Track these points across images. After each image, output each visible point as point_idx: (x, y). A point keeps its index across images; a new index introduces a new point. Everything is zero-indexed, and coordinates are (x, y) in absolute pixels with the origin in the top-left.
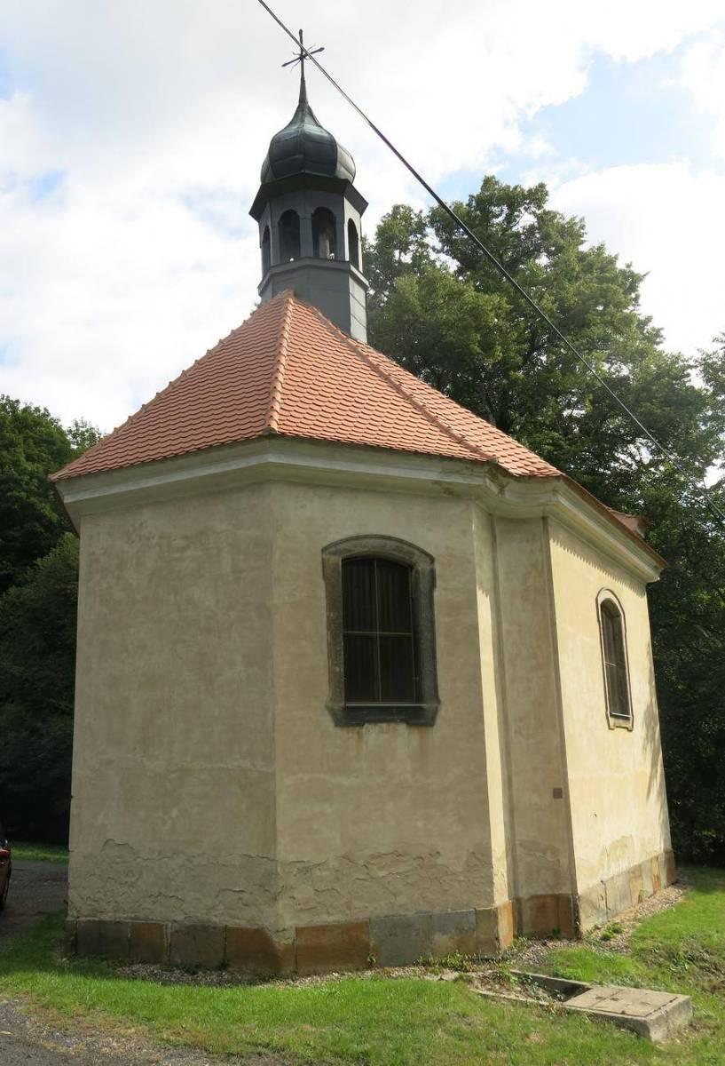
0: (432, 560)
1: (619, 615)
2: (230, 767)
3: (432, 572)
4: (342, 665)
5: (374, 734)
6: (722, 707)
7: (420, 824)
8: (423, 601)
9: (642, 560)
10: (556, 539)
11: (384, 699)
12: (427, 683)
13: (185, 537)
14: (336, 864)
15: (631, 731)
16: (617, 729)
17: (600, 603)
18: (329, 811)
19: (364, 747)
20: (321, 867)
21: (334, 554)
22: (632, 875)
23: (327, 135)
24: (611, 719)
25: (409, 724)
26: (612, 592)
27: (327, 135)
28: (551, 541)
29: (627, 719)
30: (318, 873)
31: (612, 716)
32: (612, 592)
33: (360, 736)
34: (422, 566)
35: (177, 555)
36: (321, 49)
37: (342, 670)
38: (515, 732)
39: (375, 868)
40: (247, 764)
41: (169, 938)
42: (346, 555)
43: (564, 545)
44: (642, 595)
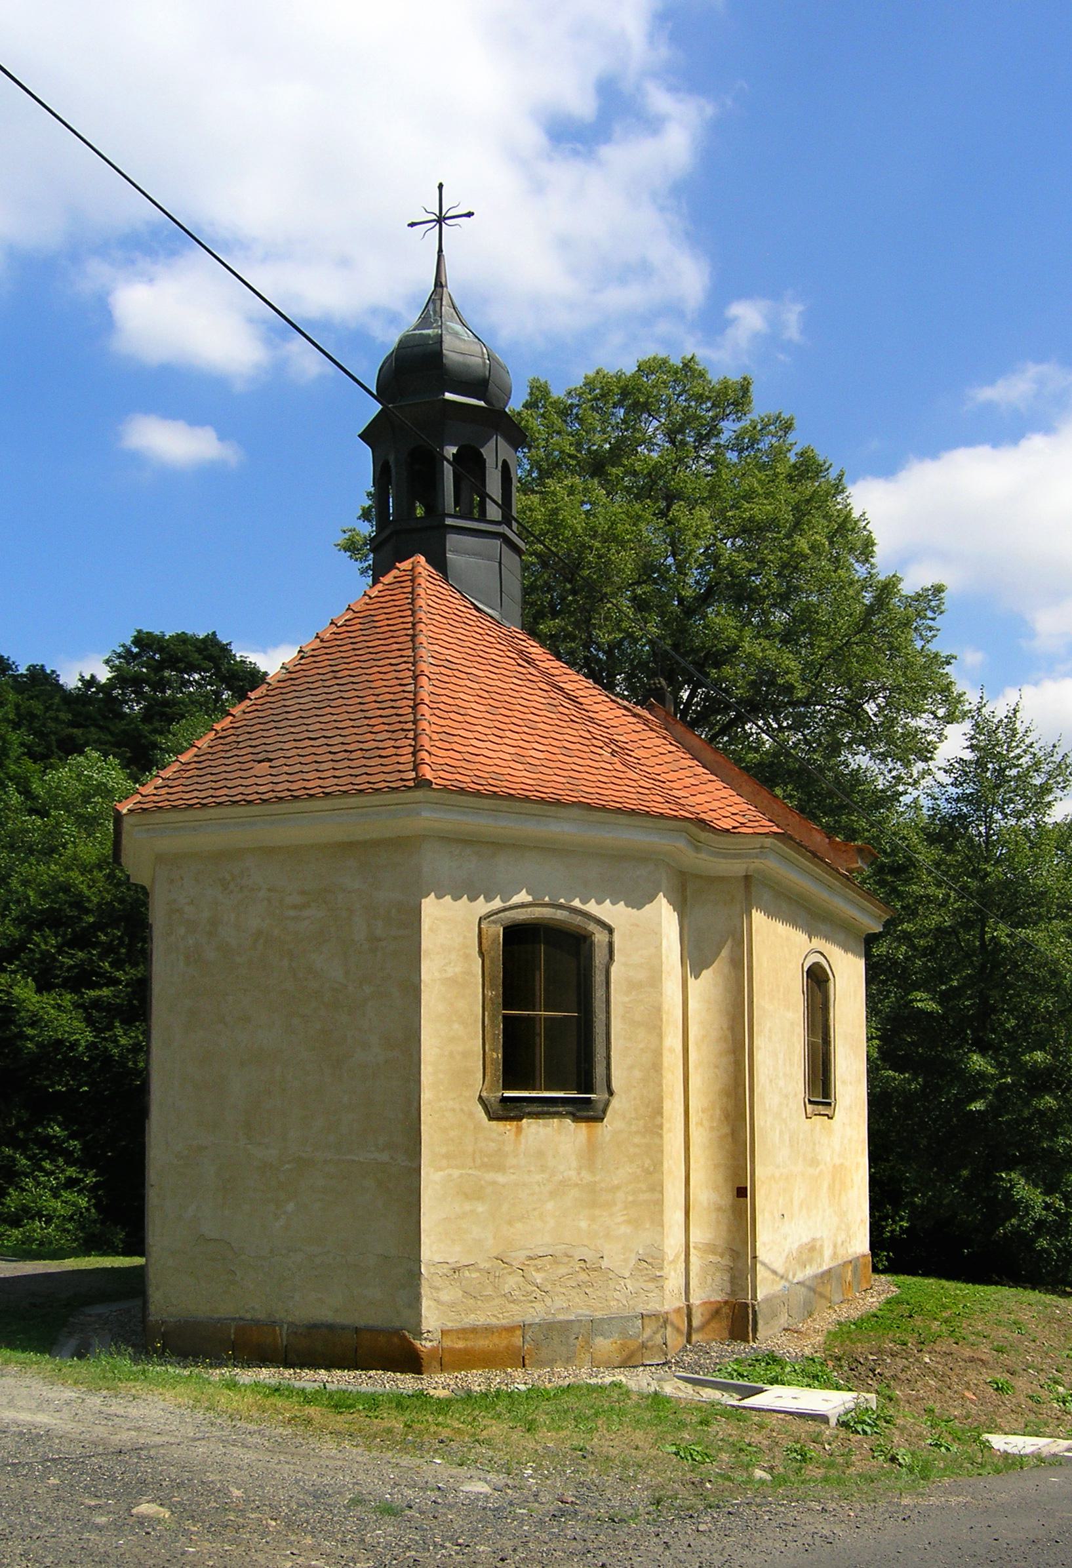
0: (611, 931)
1: (828, 980)
2: (361, 1160)
3: (611, 945)
4: (501, 1051)
5: (535, 1130)
6: (1067, 767)
7: (583, 1224)
8: (599, 978)
9: (863, 909)
10: (761, 908)
11: (547, 1089)
12: (599, 1071)
13: (303, 893)
14: (487, 1265)
15: (832, 1118)
16: (814, 1117)
17: (806, 969)
18: (480, 1209)
19: (523, 1141)
20: (471, 1268)
21: (494, 922)
22: (820, 1281)
23: (476, 348)
24: (808, 1106)
25: (576, 1119)
26: (822, 954)
27: (476, 348)
28: (754, 911)
29: (829, 1104)
30: (467, 1274)
31: (810, 1102)
32: (822, 954)
33: (519, 1130)
34: (600, 937)
35: (292, 913)
36: (470, 215)
37: (500, 1056)
38: (697, 1124)
39: (532, 1269)
40: (384, 1157)
41: (285, 1340)
42: (507, 923)
43: (771, 914)
44: (860, 957)
